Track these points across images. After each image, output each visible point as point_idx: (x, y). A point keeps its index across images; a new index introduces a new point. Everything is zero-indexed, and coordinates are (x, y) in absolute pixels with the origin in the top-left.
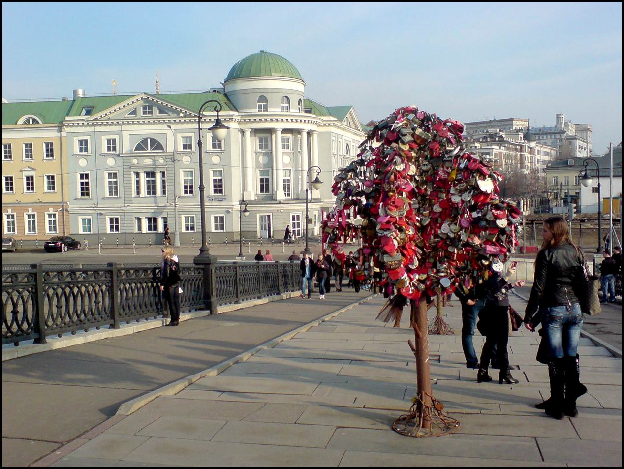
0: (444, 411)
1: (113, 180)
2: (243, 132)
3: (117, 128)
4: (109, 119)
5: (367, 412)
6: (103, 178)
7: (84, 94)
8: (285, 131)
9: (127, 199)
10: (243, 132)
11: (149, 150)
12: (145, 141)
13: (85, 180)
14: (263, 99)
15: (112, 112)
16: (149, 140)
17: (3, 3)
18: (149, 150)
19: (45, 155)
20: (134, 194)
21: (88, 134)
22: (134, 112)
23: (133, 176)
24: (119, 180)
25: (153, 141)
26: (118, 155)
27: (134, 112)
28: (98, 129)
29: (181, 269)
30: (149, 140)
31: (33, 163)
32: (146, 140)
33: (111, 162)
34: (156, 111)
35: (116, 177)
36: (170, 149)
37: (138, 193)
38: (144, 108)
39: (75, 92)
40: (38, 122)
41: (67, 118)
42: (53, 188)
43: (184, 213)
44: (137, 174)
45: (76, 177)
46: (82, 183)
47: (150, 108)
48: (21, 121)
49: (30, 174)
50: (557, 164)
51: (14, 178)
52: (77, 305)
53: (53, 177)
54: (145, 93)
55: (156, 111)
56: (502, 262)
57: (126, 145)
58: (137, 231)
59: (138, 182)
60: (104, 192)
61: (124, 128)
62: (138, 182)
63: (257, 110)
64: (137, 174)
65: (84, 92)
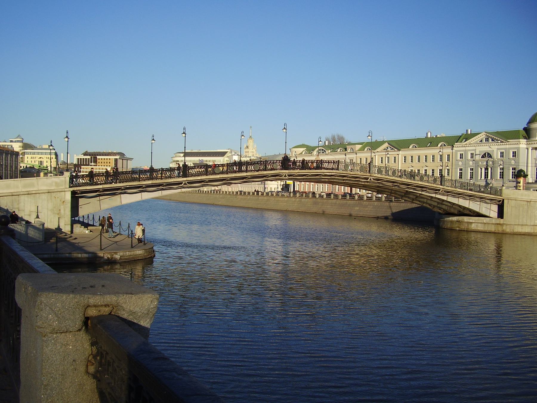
1: (472, 171)
2: (528, 149)
3: (474, 148)
4: (471, 144)
5: (96, 193)
6: (497, 171)
7: (431, 136)
9: (477, 180)
10: (528, 149)
12: (485, 154)
13: (461, 171)
15: (472, 140)
16: (487, 153)
19: (432, 161)
20: (479, 178)
21: (505, 149)
23: (480, 169)
24: (474, 171)
25: (488, 154)
26: (474, 160)
27: (481, 141)
28: (467, 148)
30: (487, 153)
31: (427, 164)
32: (486, 153)
34: (490, 140)
35: (473, 170)
37: (481, 177)
38: (486, 139)
39: (467, 131)
40: (445, 146)
41: (456, 144)
42: (449, 175)
44: (481, 169)
45: (457, 170)
46: (460, 173)
47: (488, 139)
48: (411, 147)
49: (426, 168)
52: (534, 233)
53: (449, 169)
54: (485, 132)
55: (490, 140)
60: (497, 177)
61: (477, 148)
64: (481, 169)
65: (471, 131)
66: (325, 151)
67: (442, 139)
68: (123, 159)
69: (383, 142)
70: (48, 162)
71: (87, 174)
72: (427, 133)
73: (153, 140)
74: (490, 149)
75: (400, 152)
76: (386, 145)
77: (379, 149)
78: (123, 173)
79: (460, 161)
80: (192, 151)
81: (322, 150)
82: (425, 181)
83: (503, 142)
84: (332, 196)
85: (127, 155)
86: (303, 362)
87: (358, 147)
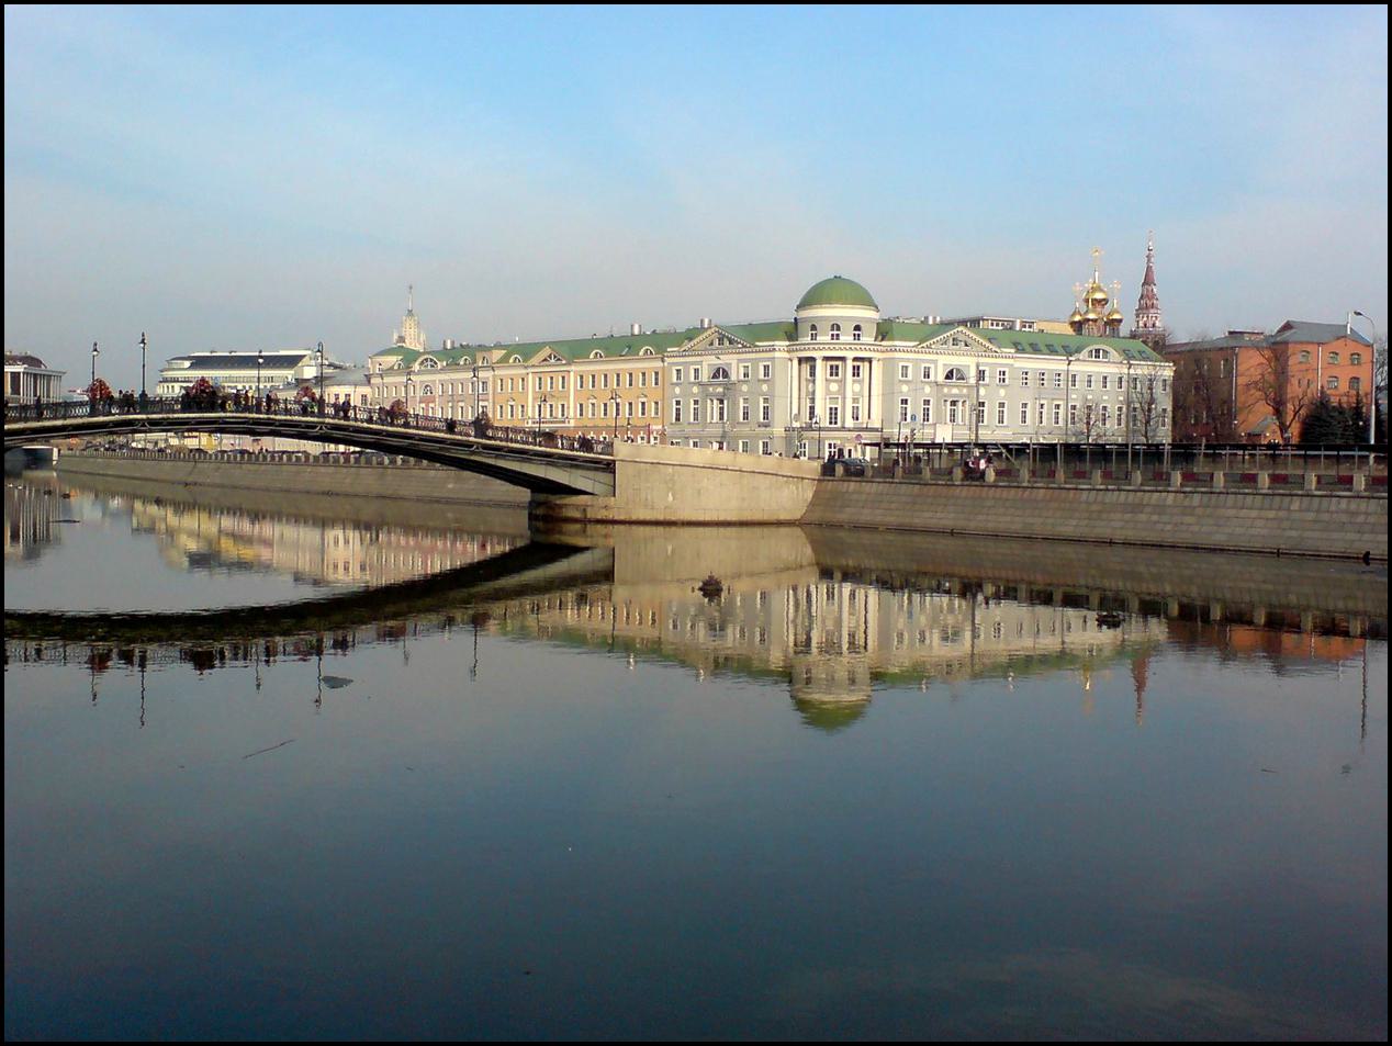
0: (804, 563)
8: (855, 359)
11: (721, 379)
14: (857, 328)
17: (7, 8)
18: (721, 379)
22: (712, 344)
23: (709, 401)
29: (96, 652)
33: (695, 389)
36: (733, 378)
39: (702, 321)
43: (741, 438)
50: (535, 434)
51: (987, 374)
55: (727, 343)
56: (378, 634)
57: (705, 376)
58: (827, 425)
59: (722, 409)
62: (722, 409)
63: (809, 338)
64: (712, 401)
66: (436, 363)
67: (642, 339)
68: (35, 375)
69: (544, 344)
70: (331, 567)
71: (191, 385)
72: (632, 326)
73: (95, 350)
74: (720, 362)
75: (573, 368)
76: (546, 351)
77: (535, 360)
78: (1169, 346)
79: (764, 381)
80: (214, 354)
81: (431, 360)
82: (312, 414)
83: (745, 347)
84: (839, 469)
85: (50, 364)
86: (463, 593)
87: (497, 354)
